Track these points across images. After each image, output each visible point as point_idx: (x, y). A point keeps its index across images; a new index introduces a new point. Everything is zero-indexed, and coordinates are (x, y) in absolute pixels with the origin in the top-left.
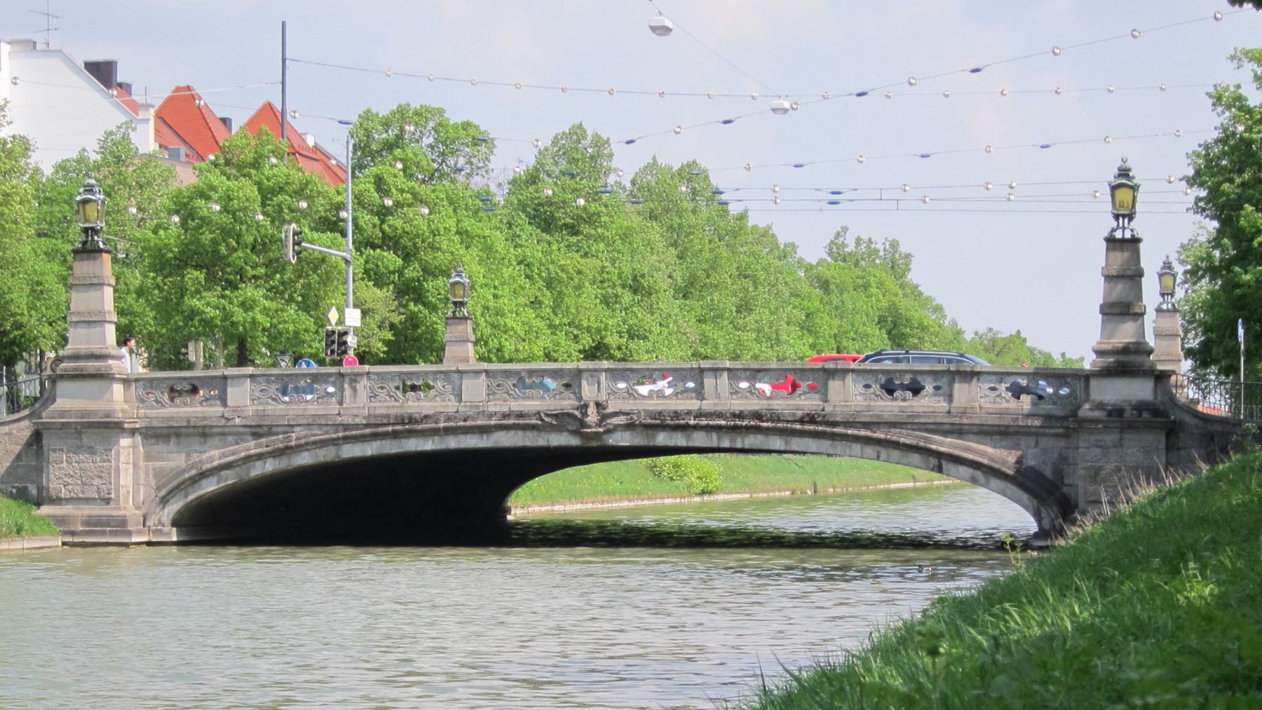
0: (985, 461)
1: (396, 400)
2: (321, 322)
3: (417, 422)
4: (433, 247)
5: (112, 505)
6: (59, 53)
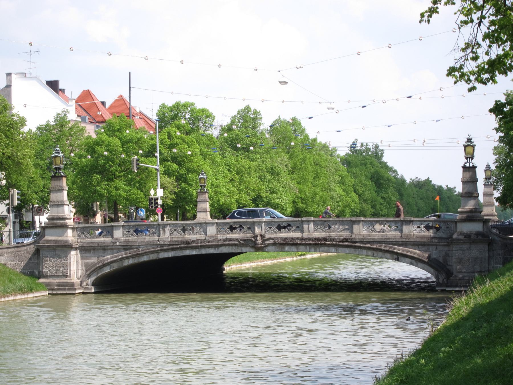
0: (416, 256)
1: (181, 235)
2: (147, 195)
3: (189, 243)
4: (191, 161)
5: (68, 278)
6: (36, 77)
